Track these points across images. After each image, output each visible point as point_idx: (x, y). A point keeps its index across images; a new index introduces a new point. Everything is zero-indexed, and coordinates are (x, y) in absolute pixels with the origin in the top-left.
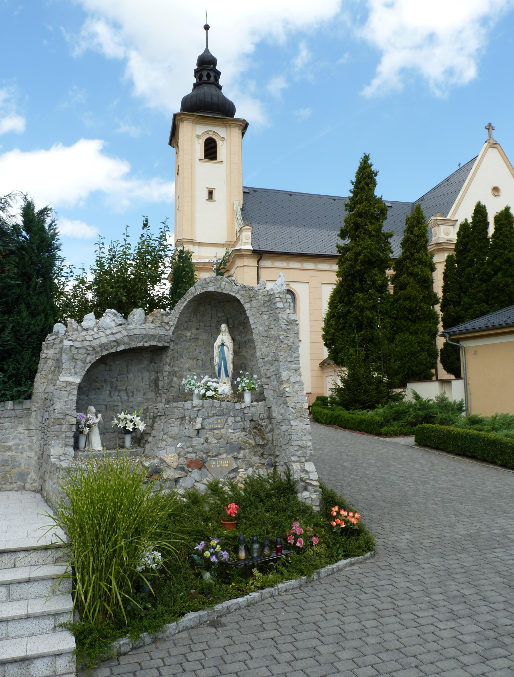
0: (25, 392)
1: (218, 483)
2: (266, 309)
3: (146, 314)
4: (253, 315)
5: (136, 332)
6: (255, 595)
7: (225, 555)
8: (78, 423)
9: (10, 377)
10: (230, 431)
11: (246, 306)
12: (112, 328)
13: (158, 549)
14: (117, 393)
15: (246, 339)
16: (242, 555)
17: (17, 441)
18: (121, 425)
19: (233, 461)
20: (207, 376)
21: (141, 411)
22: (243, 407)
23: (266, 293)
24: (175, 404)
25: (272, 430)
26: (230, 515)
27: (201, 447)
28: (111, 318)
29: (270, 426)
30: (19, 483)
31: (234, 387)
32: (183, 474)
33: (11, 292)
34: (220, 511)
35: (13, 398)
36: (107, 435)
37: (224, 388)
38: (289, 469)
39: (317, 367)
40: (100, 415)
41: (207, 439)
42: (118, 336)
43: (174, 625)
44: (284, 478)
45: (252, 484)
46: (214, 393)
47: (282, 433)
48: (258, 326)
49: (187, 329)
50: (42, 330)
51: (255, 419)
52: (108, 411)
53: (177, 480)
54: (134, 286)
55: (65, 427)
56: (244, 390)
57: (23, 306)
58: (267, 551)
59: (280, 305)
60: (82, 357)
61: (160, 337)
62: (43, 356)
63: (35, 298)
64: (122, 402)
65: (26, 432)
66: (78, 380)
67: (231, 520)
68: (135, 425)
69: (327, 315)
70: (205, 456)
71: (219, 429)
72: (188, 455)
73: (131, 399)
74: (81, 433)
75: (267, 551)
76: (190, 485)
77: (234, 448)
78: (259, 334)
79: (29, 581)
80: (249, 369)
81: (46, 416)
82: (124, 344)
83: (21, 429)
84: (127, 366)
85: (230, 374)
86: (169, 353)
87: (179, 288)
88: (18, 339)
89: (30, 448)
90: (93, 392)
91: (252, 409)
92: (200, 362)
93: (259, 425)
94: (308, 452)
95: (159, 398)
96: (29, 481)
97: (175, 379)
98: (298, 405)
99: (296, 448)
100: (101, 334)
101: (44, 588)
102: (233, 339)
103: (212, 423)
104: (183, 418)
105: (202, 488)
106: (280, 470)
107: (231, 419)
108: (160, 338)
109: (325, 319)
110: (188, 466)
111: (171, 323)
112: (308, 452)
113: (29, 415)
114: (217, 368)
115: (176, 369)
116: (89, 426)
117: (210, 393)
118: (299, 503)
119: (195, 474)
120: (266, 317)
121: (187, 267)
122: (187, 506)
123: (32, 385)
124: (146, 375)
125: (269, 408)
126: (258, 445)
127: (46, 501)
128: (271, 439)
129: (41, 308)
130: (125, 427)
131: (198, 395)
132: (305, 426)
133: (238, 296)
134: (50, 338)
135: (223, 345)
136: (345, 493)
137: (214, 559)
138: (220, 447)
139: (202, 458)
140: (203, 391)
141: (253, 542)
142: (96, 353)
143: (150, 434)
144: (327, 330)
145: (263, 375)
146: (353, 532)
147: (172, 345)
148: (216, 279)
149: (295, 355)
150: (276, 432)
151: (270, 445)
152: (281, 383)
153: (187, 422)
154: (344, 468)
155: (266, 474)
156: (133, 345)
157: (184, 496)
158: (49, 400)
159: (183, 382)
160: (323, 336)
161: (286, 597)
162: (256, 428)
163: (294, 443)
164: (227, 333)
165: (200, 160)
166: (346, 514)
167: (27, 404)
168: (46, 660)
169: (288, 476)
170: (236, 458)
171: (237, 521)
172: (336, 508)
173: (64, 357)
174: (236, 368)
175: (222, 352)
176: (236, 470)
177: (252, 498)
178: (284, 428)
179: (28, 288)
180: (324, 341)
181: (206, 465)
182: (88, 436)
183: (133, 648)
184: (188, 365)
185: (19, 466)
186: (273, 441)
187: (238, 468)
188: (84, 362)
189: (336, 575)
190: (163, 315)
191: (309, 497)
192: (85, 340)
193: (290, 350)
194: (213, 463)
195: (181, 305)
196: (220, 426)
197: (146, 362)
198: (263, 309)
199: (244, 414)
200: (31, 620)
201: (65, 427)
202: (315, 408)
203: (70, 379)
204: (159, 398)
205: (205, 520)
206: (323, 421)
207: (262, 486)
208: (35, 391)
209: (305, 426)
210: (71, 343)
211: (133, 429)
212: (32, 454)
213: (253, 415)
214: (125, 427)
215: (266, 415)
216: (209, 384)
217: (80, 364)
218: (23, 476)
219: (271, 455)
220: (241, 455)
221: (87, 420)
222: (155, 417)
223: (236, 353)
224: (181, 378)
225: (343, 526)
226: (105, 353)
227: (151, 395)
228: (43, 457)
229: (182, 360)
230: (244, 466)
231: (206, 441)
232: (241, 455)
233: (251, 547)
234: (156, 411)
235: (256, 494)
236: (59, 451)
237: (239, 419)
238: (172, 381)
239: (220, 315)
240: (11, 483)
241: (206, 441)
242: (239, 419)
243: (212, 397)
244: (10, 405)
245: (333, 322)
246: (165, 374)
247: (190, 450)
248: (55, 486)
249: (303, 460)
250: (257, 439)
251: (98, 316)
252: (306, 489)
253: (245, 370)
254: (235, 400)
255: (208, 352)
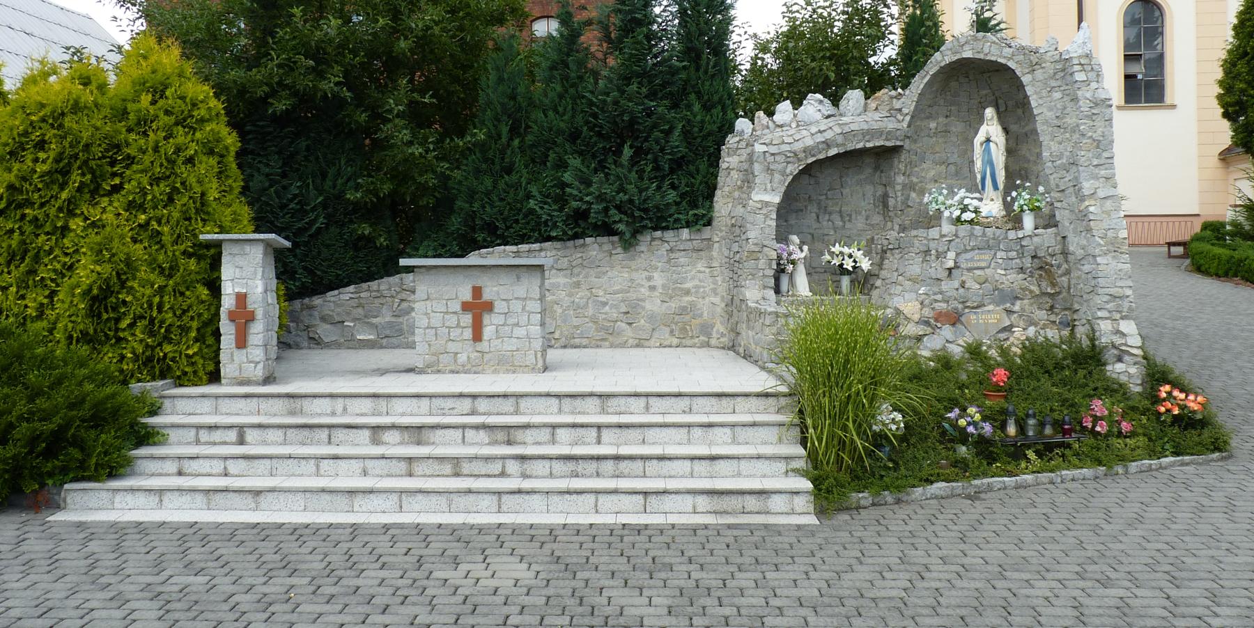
0: (704, 215)
1: (980, 345)
2: (1059, 83)
3: (867, 98)
4: (1036, 93)
5: (853, 127)
6: (1029, 478)
7: (987, 428)
8: (779, 257)
9: (683, 196)
10: (999, 271)
11: (1026, 79)
12: (817, 122)
13: (896, 408)
14: (827, 217)
15: (1027, 128)
16: (1012, 430)
17: (696, 282)
18: (836, 262)
19: (1004, 315)
20: (963, 190)
21: (863, 243)
22: (1021, 236)
23: (1057, 57)
24: (914, 233)
25: (1068, 272)
26: (997, 384)
27: (955, 293)
28: (814, 106)
29: (1065, 266)
30: (702, 338)
31: (1008, 206)
32: (929, 330)
33: (677, 77)
34: (982, 382)
35: (688, 225)
36: (816, 277)
37: (992, 207)
38: (1093, 330)
39: (1214, 161)
40: (805, 248)
41: (964, 282)
42: (829, 135)
43: (920, 490)
44: (1086, 343)
45: (1030, 348)
46: (974, 215)
47: (1084, 276)
48: (1045, 110)
49: (930, 117)
50: (720, 129)
51: (1041, 254)
52: (817, 241)
53: (919, 339)
54: (846, 55)
55: (762, 263)
56: (1022, 211)
57: (693, 96)
58: (1048, 430)
59: (1080, 77)
60: (780, 167)
61: (889, 133)
62: (723, 165)
63: (707, 83)
64: (835, 229)
65: (707, 270)
66: (777, 199)
67: (999, 391)
68: (855, 261)
69: (1229, 52)
70: (960, 306)
71: (982, 268)
72: (936, 305)
73: (848, 225)
74: (783, 271)
75: (1048, 430)
76: (939, 347)
77: (1006, 297)
78: (1046, 122)
79: (754, 424)
80: (1033, 178)
81: (735, 247)
82: (838, 146)
83: (700, 266)
84: (841, 177)
85: (1001, 186)
86: (903, 156)
87: (916, 53)
88: (689, 143)
89: (714, 291)
90: (794, 215)
91: (1035, 239)
92: (952, 168)
93: (1047, 264)
94: (1126, 305)
95: (889, 224)
96: (714, 335)
97: (913, 195)
98: (1110, 234)
99: (1106, 298)
100: (804, 132)
101: (771, 434)
102: (1006, 130)
103: (972, 260)
104: (927, 252)
105: (956, 350)
106: (1081, 331)
107: (1000, 254)
108: (889, 134)
109: (1225, 61)
110: (936, 320)
111: (905, 111)
112: (1126, 305)
113: (710, 248)
114: (979, 177)
115: (915, 180)
116: (793, 262)
117: (968, 216)
118: (1107, 379)
119: (947, 331)
120: (1057, 95)
121: (928, 19)
122: (936, 371)
123: (711, 207)
124: (869, 189)
125: (1064, 237)
126: (1044, 294)
127: (744, 357)
128: (1066, 285)
129: (716, 98)
130: (841, 265)
131: (950, 218)
132: (1120, 266)
133: (1011, 64)
134: (731, 140)
135: (988, 140)
136: (1179, 364)
137: (971, 429)
138: (983, 295)
139: (956, 309)
140: (957, 213)
141: (1028, 416)
142: (799, 160)
143: (877, 276)
144: (1228, 84)
145: (1053, 186)
146: (1187, 422)
147: (907, 144)
148: (976, 39)
149: (1106, 155)
150: (1074, 274)
151: (1064, 294)
152: (1082, 199)
153: (933, 257)
154: (1227, 349)
155: (1057, 337)
156: (850, 147)
157: (930, 359)
158: (738, 229)
159: (926, 200)
160: (1220, 97)
161: (1069, 485)
162: (1042, 268)
163: (1100, 291)
164: (995, 121)
165: (1119, 108)
166: (1182, 396)
167: (707, 233)
168: (783, 496)
169: (1092, 340)
170: (1009, 312)
171: (1006, 391)
172: (1168, 388)
173: (757, 168)
174: (1010, 175)
175: (987, 151)
176: (1009, 329)
177: (1034, 369)
178: (1086, 268)
179: (697, 70)
180: (1223, 107)
181: (963, 319)
182: (791, 276)
183: (873, 504)
184: (932, 173)
185: (701, 316)
186: (1069, 288)
187: (1012, 326)
188: (783, 173)
189: (1154, 473)
190: (892, 98)
191: (1127, 372)
192: (783, 142)
193: (1098, 147)
194: (973, 317)
195: (919, 83)
196: (983, 264)
197: (869, 170)
198: (1053, 83)
199: (1022, 246)
200: (762, 461)
201: (762, 263)
202: (1195, 245)
203: (767, 198)
204: (889, 224)
205: (960, 388)
206: (1212, 271)
207: (1048, 354)
208: (716, 214)
209: (1120, 266)
210: (764, 148)
211: (854, 267)
212: (717, 300)
213: (1036, 248)
214: (841, 265)
215: (1058, 249)
216: (966, 201)
217: (777, 177)
218: (706, 329)
219: (1066, 309)
220: (1017, 308)
221: (790, 254)
222: (884, 252)
223: (1010, 152)
224: (922, 193)
225: (1176, 412)
226: (810, 160)
227: (877, 219)
228: (734, 304)
229: (924, 165)
230: (1022, 324)
231: (963, 285)
232: (1017, 308)
233: (1026, 423)
234: (886, 242)
235: (1039, 363)
236: (756, 294)
237: (1014, 254)
238: (907, 198)
239: (984, 92)
240: (692, 337)
241: (963, 285)
242: (1014, 254)
243: (971, 222)
244: (685, 233)
245: (1242, 67)
246: (898, 187)
247: (939, 297)
248: (758, 337)
249: (1118, 316)
250: (1044, 284)
251: (797, 104)
252: (1120, 360)
253: (1026, 178)
254: (1010, 226)
255: (965, 152)
